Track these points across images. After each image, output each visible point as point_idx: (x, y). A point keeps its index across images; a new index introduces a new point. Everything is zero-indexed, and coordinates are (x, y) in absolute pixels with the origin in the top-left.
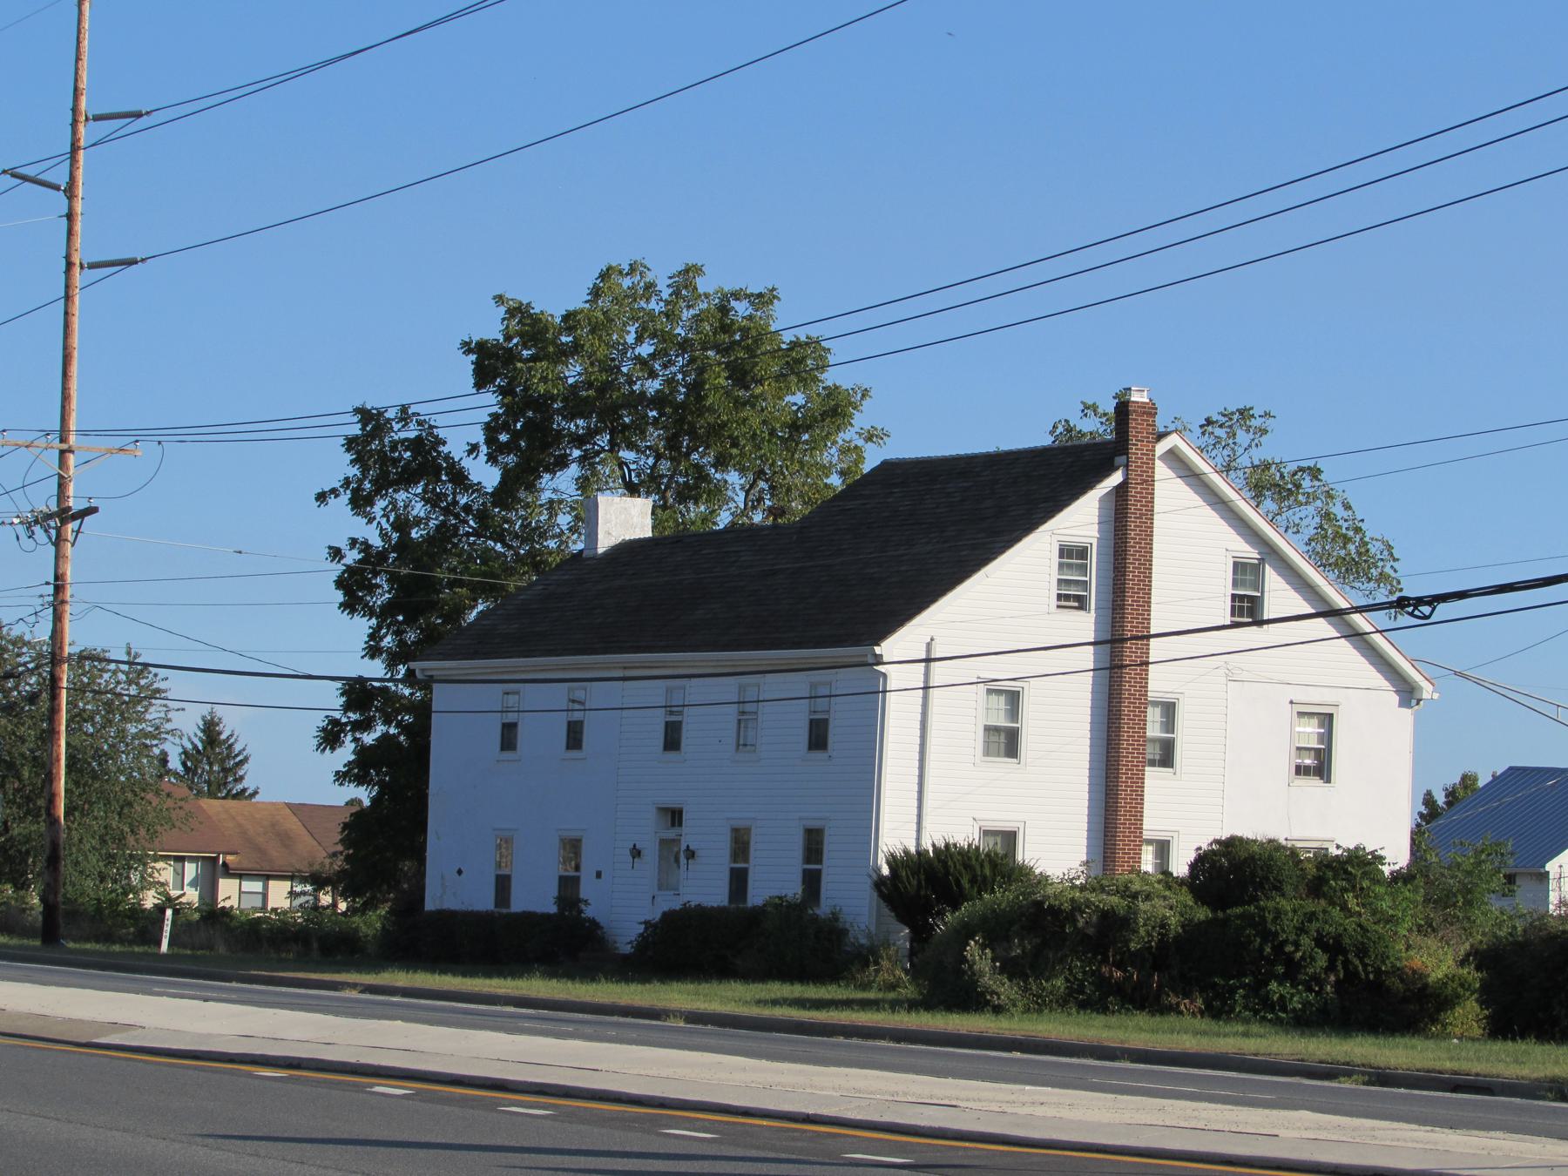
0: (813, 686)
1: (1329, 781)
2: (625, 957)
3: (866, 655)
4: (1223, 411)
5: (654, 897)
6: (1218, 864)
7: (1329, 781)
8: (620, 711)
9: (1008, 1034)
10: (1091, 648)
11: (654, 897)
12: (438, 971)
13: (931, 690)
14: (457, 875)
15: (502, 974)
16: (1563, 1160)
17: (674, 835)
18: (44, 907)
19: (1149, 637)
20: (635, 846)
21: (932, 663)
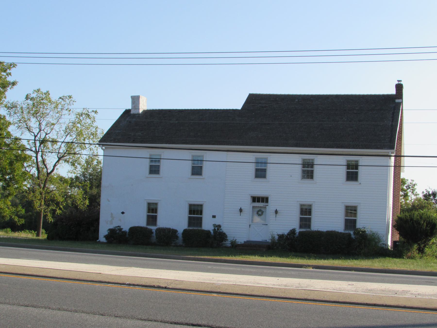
0: (193, 156)
1: (251, 196)
2: (230, 247)
3: (389, 153)
4: (16, 102)
5: (250, 225)
6: (59, 214)
7: (251, 196)
8: (151, 158)
9: (325, 265)
10: (103, 156)
11: (250, 225)
12: (326, 259)
13: (268, 164)
14: (124, 214)
15: (320, 258)
16: (0, 274)
17: (263, 205)
18: (44, 229)
19: (103, 156)
20: (241, 208)
21: (391, 157)
